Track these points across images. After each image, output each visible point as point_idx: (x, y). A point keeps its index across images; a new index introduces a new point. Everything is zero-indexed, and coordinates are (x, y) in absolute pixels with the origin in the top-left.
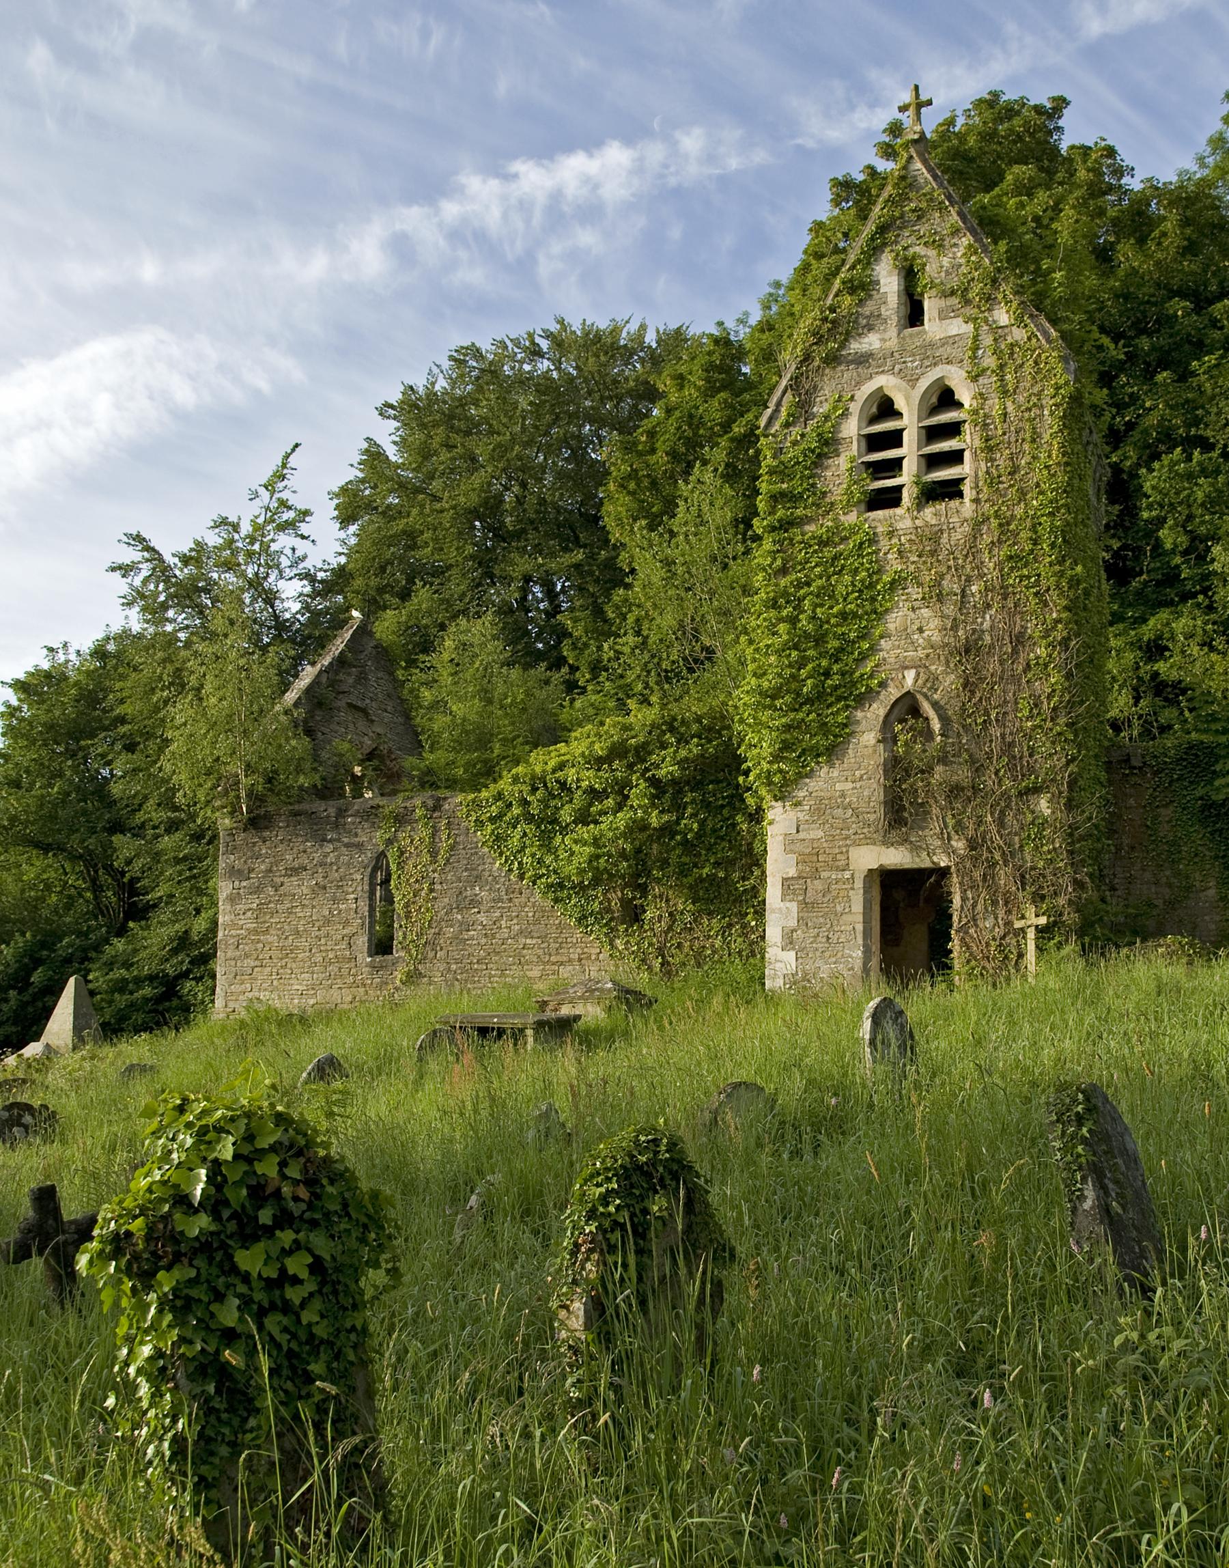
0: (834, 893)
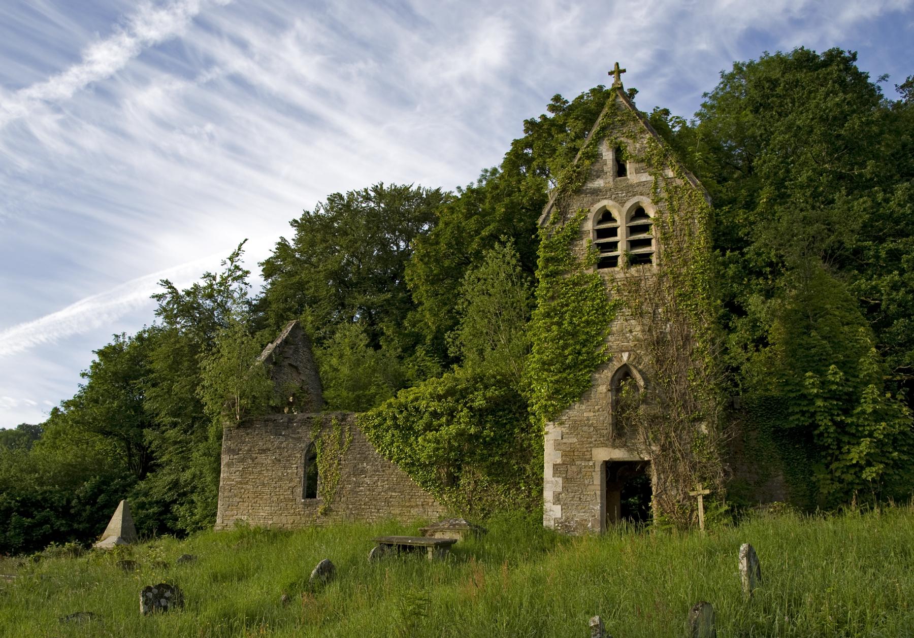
0: (584, 473)
